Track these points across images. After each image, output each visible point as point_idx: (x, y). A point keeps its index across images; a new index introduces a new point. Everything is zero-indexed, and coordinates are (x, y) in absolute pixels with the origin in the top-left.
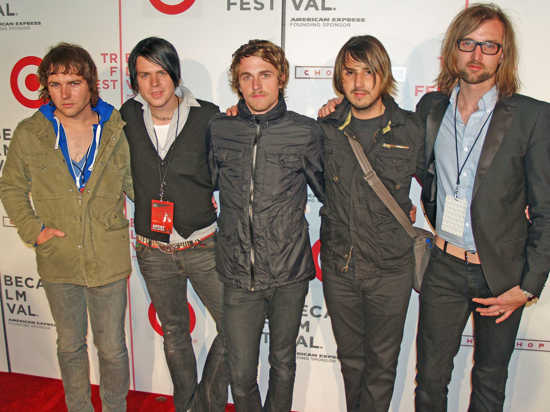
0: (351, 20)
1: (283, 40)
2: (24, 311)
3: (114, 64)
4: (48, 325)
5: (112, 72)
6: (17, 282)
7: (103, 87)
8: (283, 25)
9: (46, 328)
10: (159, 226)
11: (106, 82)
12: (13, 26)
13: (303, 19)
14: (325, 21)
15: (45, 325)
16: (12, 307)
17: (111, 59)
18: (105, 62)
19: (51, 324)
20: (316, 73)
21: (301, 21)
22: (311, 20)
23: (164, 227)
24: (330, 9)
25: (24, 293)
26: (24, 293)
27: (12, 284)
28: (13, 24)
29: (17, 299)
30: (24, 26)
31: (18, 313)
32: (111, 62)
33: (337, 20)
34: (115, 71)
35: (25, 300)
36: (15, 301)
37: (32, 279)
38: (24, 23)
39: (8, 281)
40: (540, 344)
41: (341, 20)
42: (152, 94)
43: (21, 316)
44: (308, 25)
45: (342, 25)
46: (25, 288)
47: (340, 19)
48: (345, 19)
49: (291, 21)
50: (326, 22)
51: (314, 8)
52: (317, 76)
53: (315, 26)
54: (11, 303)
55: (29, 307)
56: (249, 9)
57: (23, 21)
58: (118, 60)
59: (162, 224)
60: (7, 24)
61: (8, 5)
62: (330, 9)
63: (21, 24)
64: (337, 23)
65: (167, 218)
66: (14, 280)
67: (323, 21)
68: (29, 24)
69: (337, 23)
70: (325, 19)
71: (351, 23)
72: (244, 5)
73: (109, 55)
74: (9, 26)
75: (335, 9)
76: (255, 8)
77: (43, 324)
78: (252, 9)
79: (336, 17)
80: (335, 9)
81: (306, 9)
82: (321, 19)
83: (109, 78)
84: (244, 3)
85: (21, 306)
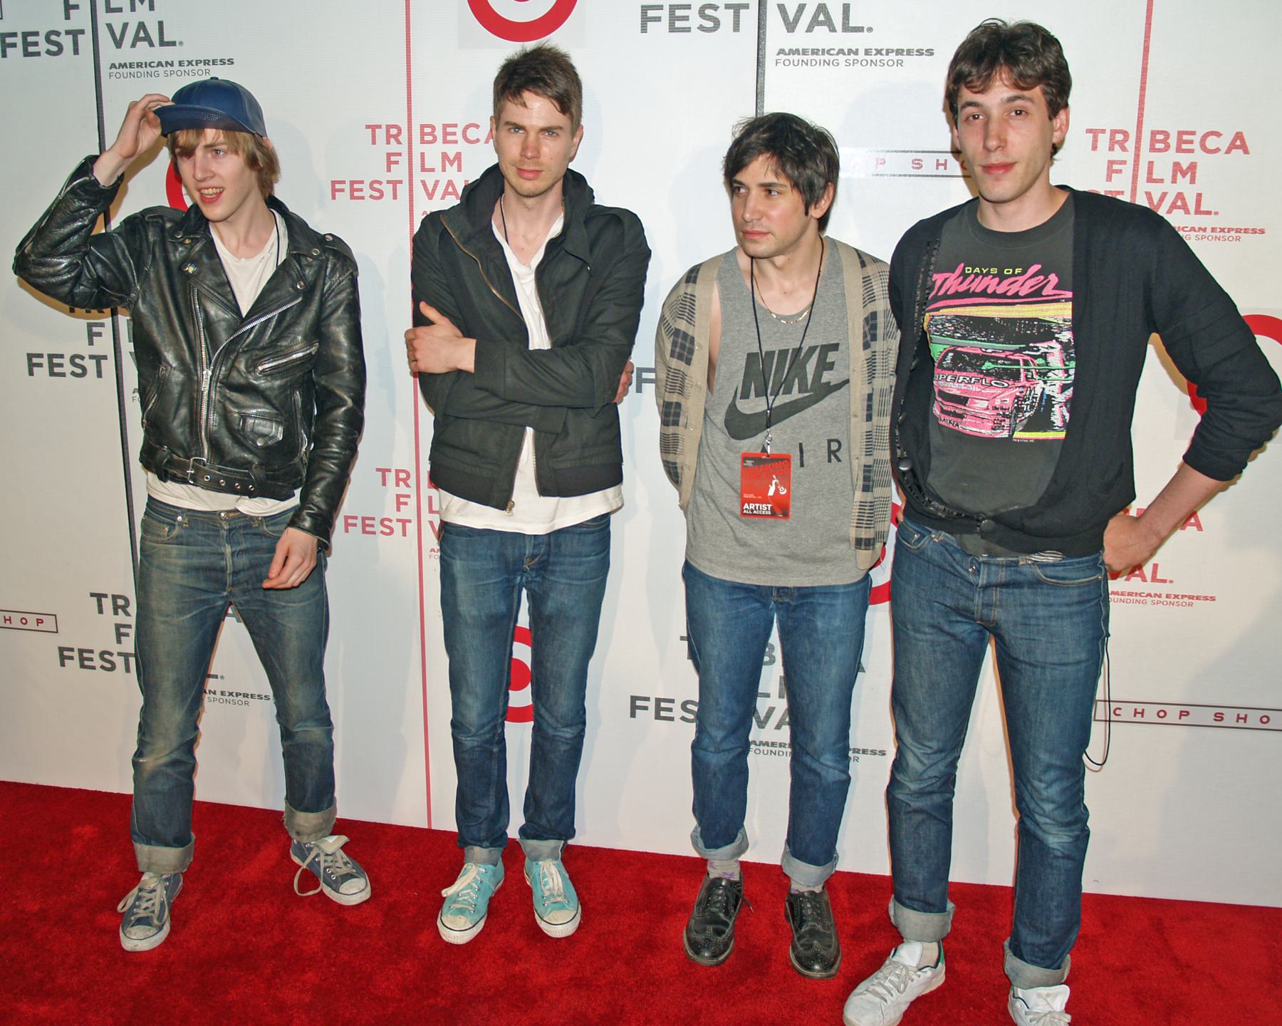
0: (905, 53)
1: (759, 96)
3: (394, 147)
5: (389, 163)
6: (445, 134)
7: (372, 197)
8: (760, 63)
9: (240, 703)
10: (757, 505)
11: (376, 186)
12: (172, 68)
13: (130, 64)
14: (849, 54)
15: (237, 696)
17: (389, 136)
18: (374, 142)
19: (252, 695)
20: (938, 165)
21: (799, 54)
22: (820, 53)
23: (769, 506)
24: (860, 29)
25: (458, 156)
26: (458, 156)
27: (1167, 147)
28: (172, 65)
30: (196, 68)
32: (388, 142)
33: (186, 63)
34: (397, 163)
35: (459, 169)
36: (438, 174)
40: (1181, 712)
41: (884, 52)
44: (814, 63)
45: (885, 62)
47: (882, 50)
48: (893, 51)
49: (778, 54)
50: (852, 57)
51: (146, 43)
52: (941, 171)
53: (829, 64)
54: (430, 179)
56: (688, 30)
57: (886, 47)
58: (404, 137)
59: (765, 500)
60: (160, 64)
61: (161, 24)
62: (860, 29)
63: (190, 63)
64: (874, 58)
65: (776, 488)
67: (844, 54)
68: (209, 65)
69: (874, 58)
70: (850, 51)
71: (905, 58)
72: (676, 22)
73: (384, 128)
74: (165, 68)
75: (870, 30)
76: (701, 28)
77: (234, 694)
78: (694, 30)
79: (874, 46)
80: (870, 30)
81: (810, 29)
82: (841, 51)
83: (384, 176)
84: (650, 18)
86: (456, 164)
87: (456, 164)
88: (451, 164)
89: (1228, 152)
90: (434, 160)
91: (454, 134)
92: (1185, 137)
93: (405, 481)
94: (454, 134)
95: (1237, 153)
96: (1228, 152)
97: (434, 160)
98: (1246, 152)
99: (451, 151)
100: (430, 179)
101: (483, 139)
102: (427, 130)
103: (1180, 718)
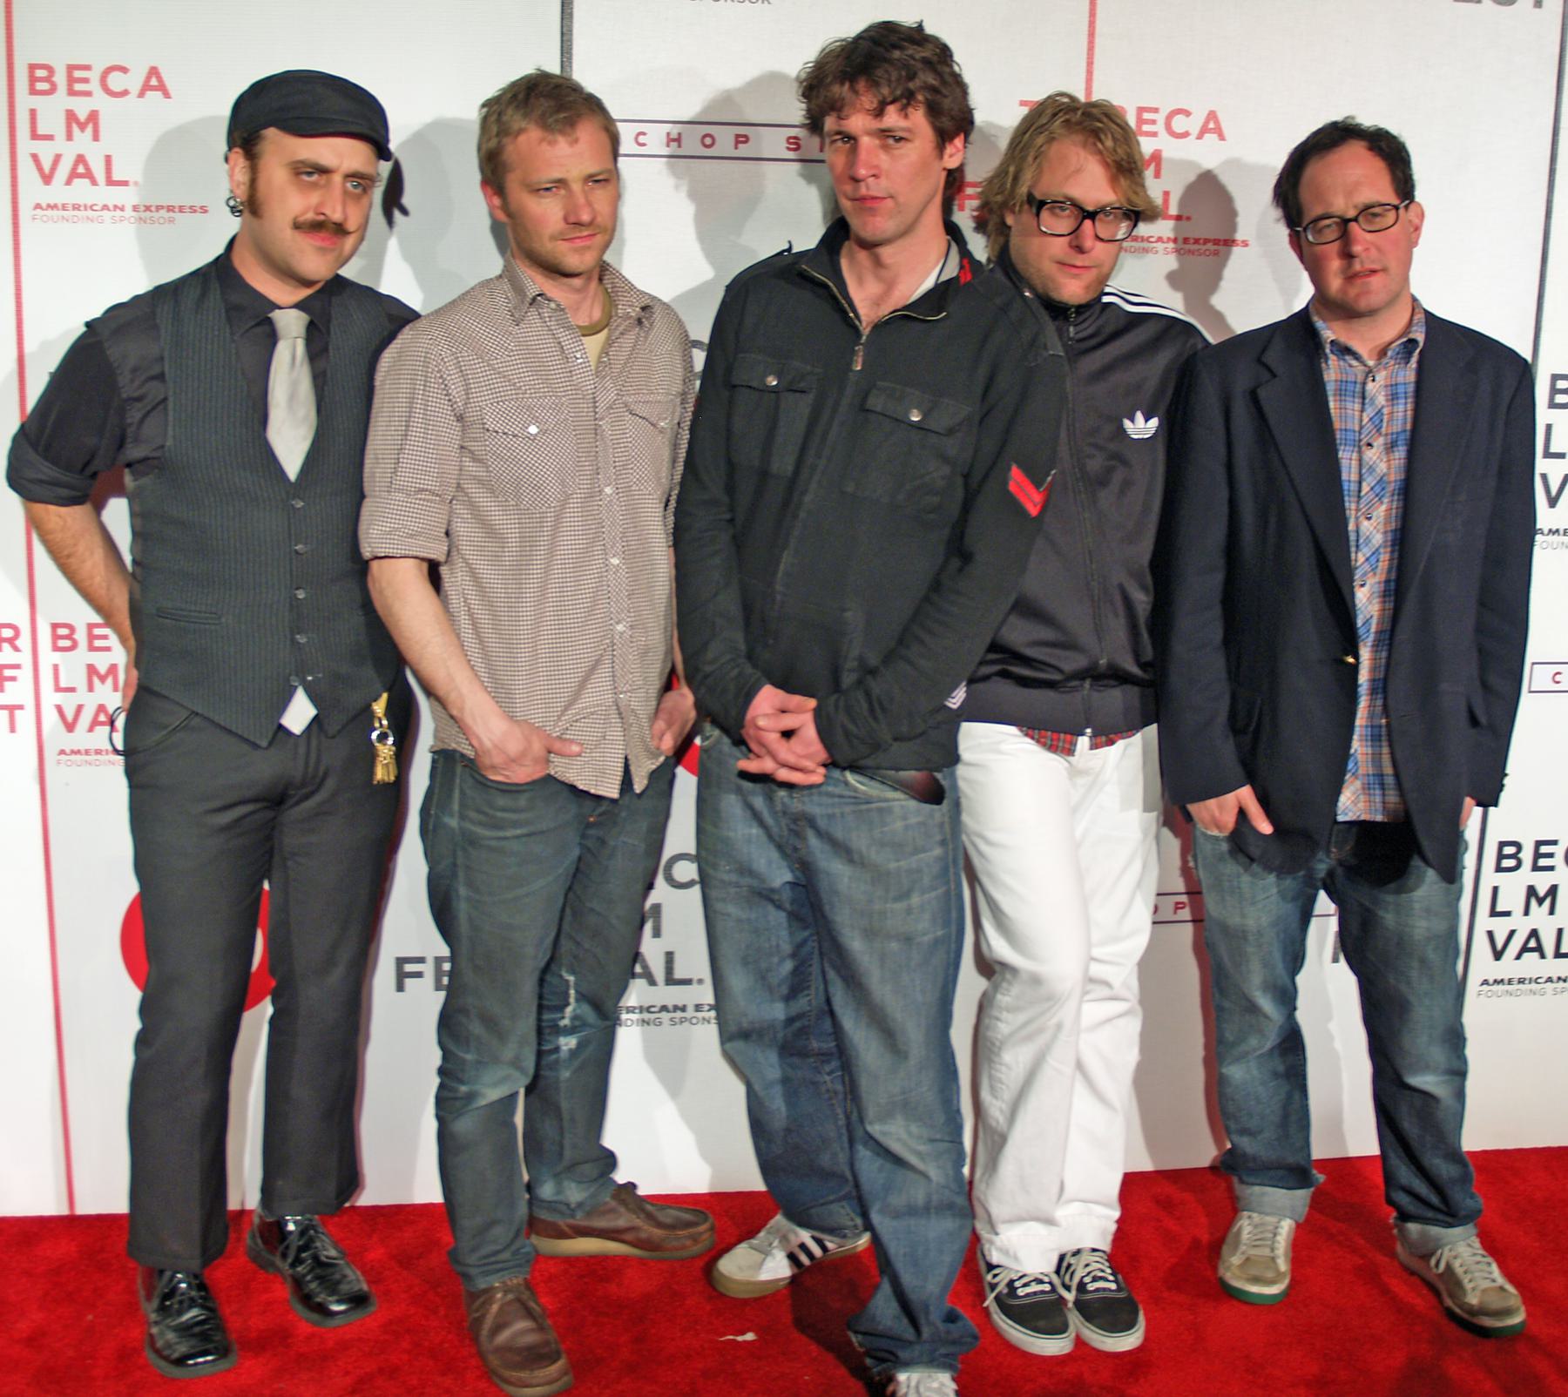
2: (89, 175)
4: (169, 210)
6: (71, 80)
14: (674, 1011)
16: (70, 716)
25: (93, 117)
26: (93, 117)
27: (53, 90)
29: (69, 137)
31: (91, 729)
35: (96, 137)
36: (60, 145)
37: (124, 70)
38: (159, 208)
39: (42, 80)
42: (462, 447)
43: (82, 191)
46: (100, 101)
50: (679, 1014)
54: (46, 151)
55: (108, 159)
66: (60, 78)
70: (676, 1008)
85: (81, 159)
86: (90, 129)
87: (90, 129)
88: (82, 127)
89: (1200, 137)
90: (51, 121)
91: (1153, 122)
92: (1146, 116)
93: (11, 641)
94: (1153, 122)
95: (154, 96)
96: (1200, 137)
97: (51, 121)
98: (1222, 137)
99: (82, 107)
100: (46, 151)
101: (1195, 131)
102: (40, 73)
103: (1175, 913)
